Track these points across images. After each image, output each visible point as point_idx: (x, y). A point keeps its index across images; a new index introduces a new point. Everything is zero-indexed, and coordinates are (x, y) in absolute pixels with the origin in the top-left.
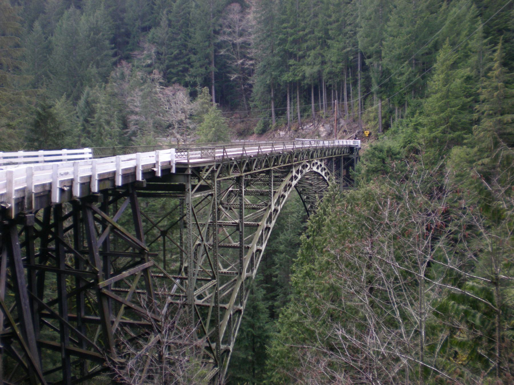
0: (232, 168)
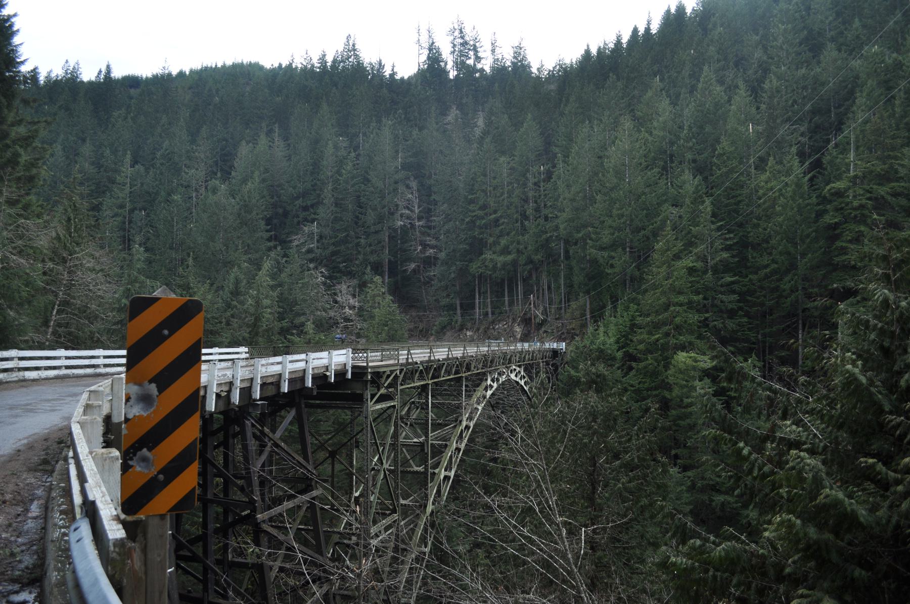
0: (417, 374)
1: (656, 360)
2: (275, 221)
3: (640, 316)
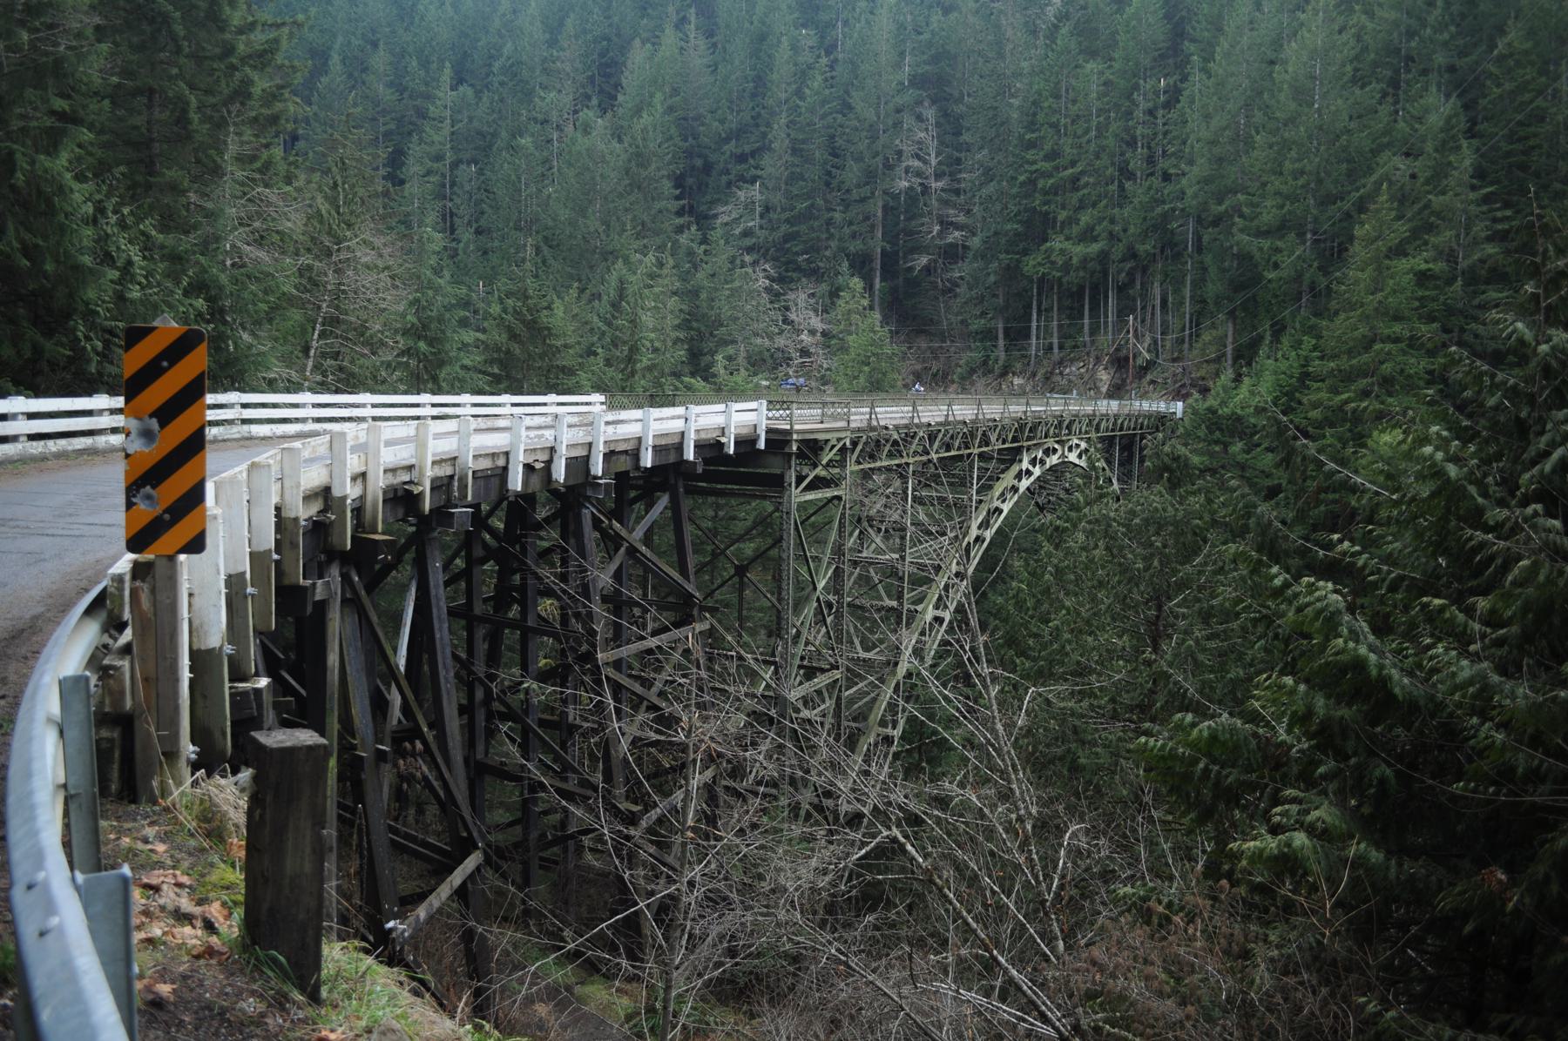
1: (1340, 439)
2: (690, 181)
3: (1322, 358)
